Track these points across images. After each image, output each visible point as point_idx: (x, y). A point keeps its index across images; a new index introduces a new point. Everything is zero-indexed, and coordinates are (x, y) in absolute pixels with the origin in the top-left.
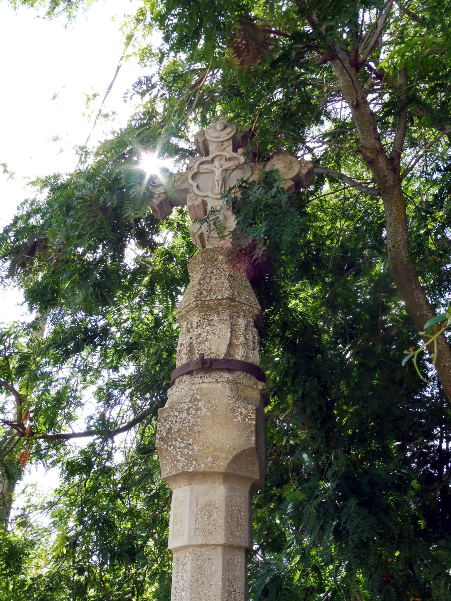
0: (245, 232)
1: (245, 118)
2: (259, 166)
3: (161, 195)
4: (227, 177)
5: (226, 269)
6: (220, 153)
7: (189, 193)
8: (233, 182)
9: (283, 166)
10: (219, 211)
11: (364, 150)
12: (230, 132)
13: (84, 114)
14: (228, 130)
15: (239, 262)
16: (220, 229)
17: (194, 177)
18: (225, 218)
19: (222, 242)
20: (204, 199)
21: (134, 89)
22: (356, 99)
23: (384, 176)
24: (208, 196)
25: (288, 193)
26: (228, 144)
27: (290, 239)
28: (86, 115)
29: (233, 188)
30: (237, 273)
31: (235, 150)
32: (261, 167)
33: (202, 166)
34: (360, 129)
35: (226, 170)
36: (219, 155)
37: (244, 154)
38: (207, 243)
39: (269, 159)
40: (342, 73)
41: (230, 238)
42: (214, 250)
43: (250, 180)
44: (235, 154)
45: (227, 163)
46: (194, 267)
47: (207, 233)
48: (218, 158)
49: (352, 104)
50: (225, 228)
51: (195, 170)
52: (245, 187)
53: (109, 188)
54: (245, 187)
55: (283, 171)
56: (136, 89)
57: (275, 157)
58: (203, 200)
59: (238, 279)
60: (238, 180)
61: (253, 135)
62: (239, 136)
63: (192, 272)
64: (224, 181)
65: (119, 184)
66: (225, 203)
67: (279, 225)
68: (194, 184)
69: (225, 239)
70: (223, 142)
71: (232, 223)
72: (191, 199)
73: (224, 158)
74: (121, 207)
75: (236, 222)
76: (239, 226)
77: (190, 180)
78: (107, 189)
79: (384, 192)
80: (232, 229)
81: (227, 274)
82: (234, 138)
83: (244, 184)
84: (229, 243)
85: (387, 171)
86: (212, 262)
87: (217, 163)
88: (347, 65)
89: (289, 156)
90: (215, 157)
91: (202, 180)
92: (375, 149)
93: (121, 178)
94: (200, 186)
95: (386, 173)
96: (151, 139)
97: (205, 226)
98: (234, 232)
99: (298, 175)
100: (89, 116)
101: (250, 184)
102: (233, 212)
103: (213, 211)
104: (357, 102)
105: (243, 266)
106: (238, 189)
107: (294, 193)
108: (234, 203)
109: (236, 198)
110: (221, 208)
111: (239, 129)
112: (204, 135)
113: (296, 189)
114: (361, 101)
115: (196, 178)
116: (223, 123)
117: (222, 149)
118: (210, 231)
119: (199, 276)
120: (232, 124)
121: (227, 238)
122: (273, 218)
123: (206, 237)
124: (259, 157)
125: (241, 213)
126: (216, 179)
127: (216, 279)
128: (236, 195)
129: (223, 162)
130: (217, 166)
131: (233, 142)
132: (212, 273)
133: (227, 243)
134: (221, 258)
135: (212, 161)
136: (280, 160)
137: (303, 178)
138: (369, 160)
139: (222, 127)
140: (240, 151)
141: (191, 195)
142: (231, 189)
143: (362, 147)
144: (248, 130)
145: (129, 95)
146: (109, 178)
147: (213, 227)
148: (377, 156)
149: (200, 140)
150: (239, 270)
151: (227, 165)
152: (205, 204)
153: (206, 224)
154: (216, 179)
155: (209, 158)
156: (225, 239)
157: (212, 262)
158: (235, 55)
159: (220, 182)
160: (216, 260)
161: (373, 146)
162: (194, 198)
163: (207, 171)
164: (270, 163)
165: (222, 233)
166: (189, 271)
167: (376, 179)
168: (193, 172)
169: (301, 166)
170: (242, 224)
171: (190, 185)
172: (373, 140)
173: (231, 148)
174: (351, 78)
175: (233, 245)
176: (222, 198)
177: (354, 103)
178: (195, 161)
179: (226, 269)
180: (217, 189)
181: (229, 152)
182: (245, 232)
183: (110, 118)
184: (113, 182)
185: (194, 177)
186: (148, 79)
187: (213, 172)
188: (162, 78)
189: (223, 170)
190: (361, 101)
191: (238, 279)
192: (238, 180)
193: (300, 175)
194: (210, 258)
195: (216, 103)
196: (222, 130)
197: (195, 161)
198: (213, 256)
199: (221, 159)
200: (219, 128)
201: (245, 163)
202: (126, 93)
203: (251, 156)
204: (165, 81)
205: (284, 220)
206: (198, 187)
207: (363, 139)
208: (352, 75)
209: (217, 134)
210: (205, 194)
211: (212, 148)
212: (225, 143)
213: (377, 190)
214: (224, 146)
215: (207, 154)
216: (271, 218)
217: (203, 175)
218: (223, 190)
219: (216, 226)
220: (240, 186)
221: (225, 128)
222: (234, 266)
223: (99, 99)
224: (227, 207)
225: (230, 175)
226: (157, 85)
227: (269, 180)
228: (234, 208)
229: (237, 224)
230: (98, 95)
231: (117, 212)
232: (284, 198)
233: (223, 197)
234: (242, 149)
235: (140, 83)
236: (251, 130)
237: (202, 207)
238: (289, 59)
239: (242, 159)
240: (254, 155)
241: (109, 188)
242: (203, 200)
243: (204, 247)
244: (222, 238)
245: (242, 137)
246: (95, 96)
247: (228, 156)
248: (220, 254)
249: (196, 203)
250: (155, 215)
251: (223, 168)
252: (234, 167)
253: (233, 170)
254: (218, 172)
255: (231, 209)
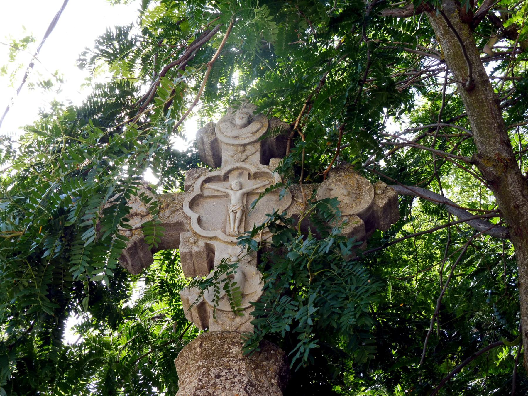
0: (278, 305)
1: (284, 107)
2: (305, 191)
3: (136, 232)
4: (250, 207)
5: (243, 371)
6: (239, 165)
7: (183, 230)
8: (259, 218)
9: (345, 193)
10: (234, 266)
11: (482, 162)
12: (257, 129)
13: (4, 70)
14: (255, 126)
15: (267, 359)
16: (235, 296)
17: (193, 204)
18: (245, 277)
19: (238, 320)
20: (210, 242)
21: (97, 47)
22: (470, 76)
23: (517, 207)
24: (216, 238)
25: (353, 239)
26: (253, 150)
27: (352, 322)
28: (9, 71)
29: (260, 228)
30: (262, 378)
31: (265, 161)
32: (308, 192)
33: (207, 185)
34: (477, 125)
35: (248, 194)
36: (237, 168)
37: (279, 170)
38: (211, 320)
39: (321, 179)
40: (446, 33)
41: (252, 313)
42: (223, 335)
43: (289, 216)
44: (264, 168)
45: (252, 182)
46: (187, 364)
47: (212, 304)
48: (236, 173)
49: (463, 85)
50: (243, 295)
51: (197, 191)
52: (280, 227)
53: (50, 228)
54: (280, 226)
55: (346, 201)
56: (101, 47)
57: (332, 175)
58: (207, 244)
59: (263, 390)
60: (268, 215)
61: (296, 134)
62: (273, 137)
63: (182, 372)
64: (245, 213)
65: (66, 220)
66: (245, 252)
67: (336, 298)
68: (194, 217)
69: (242, 316)
70: (245, 145)
71: (255, 287)
72: (186, 241)
73: (246, 173)
74: (67, 260)
75: (262, 286)
76: (267, 293)
77: (186, 209)
78: (44, 229)
79: (516, 233)
80: (255, 298)
81: (245, 380)
82: (263, 140)
83: (278, 222)
84: (248, 323)
85: (521, 198)
86: (219, 358)
87: (233, 181)
88: (455, 20)
89: (356, 176)
90: (230, 171)
91: (206, 208)
92: (501, 160)
93: (69, 211)
94: (204, 219)
95: (519, 202)
96: (125, 150)
97: (208, 294)
98: (258, 304)
99: (370, 208)
100: (12, 75)
101: (289, 221)
102: (259, 268)
103: (224, 266)
104: (472, 81)
105: (273, 366)
106: (267, 230)
107: (362, 239)
108: (260, 252)
109: (264, 243)
110: (239, 261)
111: (273, 126)
112: (213, 132)
113: (367, 231)
114: (479, 80)
115: (198, 205)
116: (247, 113)
117: (244, 157)
118: (217, 299)
119: (195, 382)
120: (261, 115)
121: (247, 315)
122: (328, 284)
123: (209, 310)
124: (305, 173)
125: (273, 271)
126: (231, 208)
127: (224, 388)
128: (265, 237)
129: (244, 179)
130: (234, 186)
131: (262, 146)
132: (218, 376)
133: (246, 323)
134: (235, 350)
135: (226, 177)
136: (340, 181)
137: (380, 214)
138: (491, 179)
139: (245, 120)
140: (275, 162)
141: (188, 234)
142: (255, 231)
143: (480, 156)
144: (287, 127)
145: (89, 57)
146: (49, 209)
147: (223, 292)
148: (506, 172)
149: (207, 140)
150: (265, 372)
151: (250, 185)
152: (210, 250)
153: (211, 288)
154: (231, 208)
155: (220, 172)
156: (242, 316)
157: (219, 358)
158: (271, 17)
159: (238, 215)
160: (227, 353)
161: (497, 155)
162: (192, 240)
163: (216, 193)
164: (324, 185)
165: (238, 304)
166: (178, 370)
167: (503, 211)
168: (192, 195)
169: (375, 193)
170: (273, 291)
171: (187, 217)
172: (498, 146)
173: (258, 156)
174: (462, 43)
175: (256, 327)
176: (240, 243)
177: (467, 83)
178: (195, 175)
179: (243, 371)
180: (233, 227)
181: (254, 163)
182: (278, 305)
183: (54, 88)
184: (55, 216)
185: (193, 204)
186: (122, 34)
187: (227, 196)
188: (145, 31)
189: (244, 194)
190: (479, 80)
191: (263, 390)
192: (268, 215)
193: (375, 209)
194: (217, 350)
195: (233, 64)
196: (245, 126)
197: (195, 175)
198: (222, 346)
199: (241, 173)
200: (238, 122)
201: (282, 184)
202: (84, 54)
203: (292, 172)
204: (151, 35)
205: (345, 288)
206: (199, 220)
207: (481, 143)
208: (463, 37)
209: (235, 133)
210: (211, 235)
211: (226, 155)
212: (248, 147)
213: (504, 229)
214: (247, 153)
215: (218, 164)
216: (323, 286)
217: (209, 200)
218: (242, 230)
219: (228, 291)
220: (272, 226)
221: (249, 122)
222: (257, 366)
223: (32, 47)
224: (249, 258)
225: (255, 203)
226: (136, 40)
227: (319, 220)
228: (259, 261)
229: (265, 289)
230: (33, 40)
231: (60, 267)
232: (346, 251)
233: (243, 241)
234: (278, 160)
235: (109, 38)
236: (292, 126)
237: (205, 256)
238: (359, 15)
239: (277, 178)
240: (297, 169)
241: (50, 228)
242: (207, 244)
243: (205, 326)
244: (238, 313)
245: (278, 139)
246: (26, 40)
247: (253, 170)
248: (233, 343)
249: (196, 249)
250: (123, 265)
251: (244, 190)
252: (263, 190)
253: (261, 195)
254: (235, 197)
255: (255, 261)
